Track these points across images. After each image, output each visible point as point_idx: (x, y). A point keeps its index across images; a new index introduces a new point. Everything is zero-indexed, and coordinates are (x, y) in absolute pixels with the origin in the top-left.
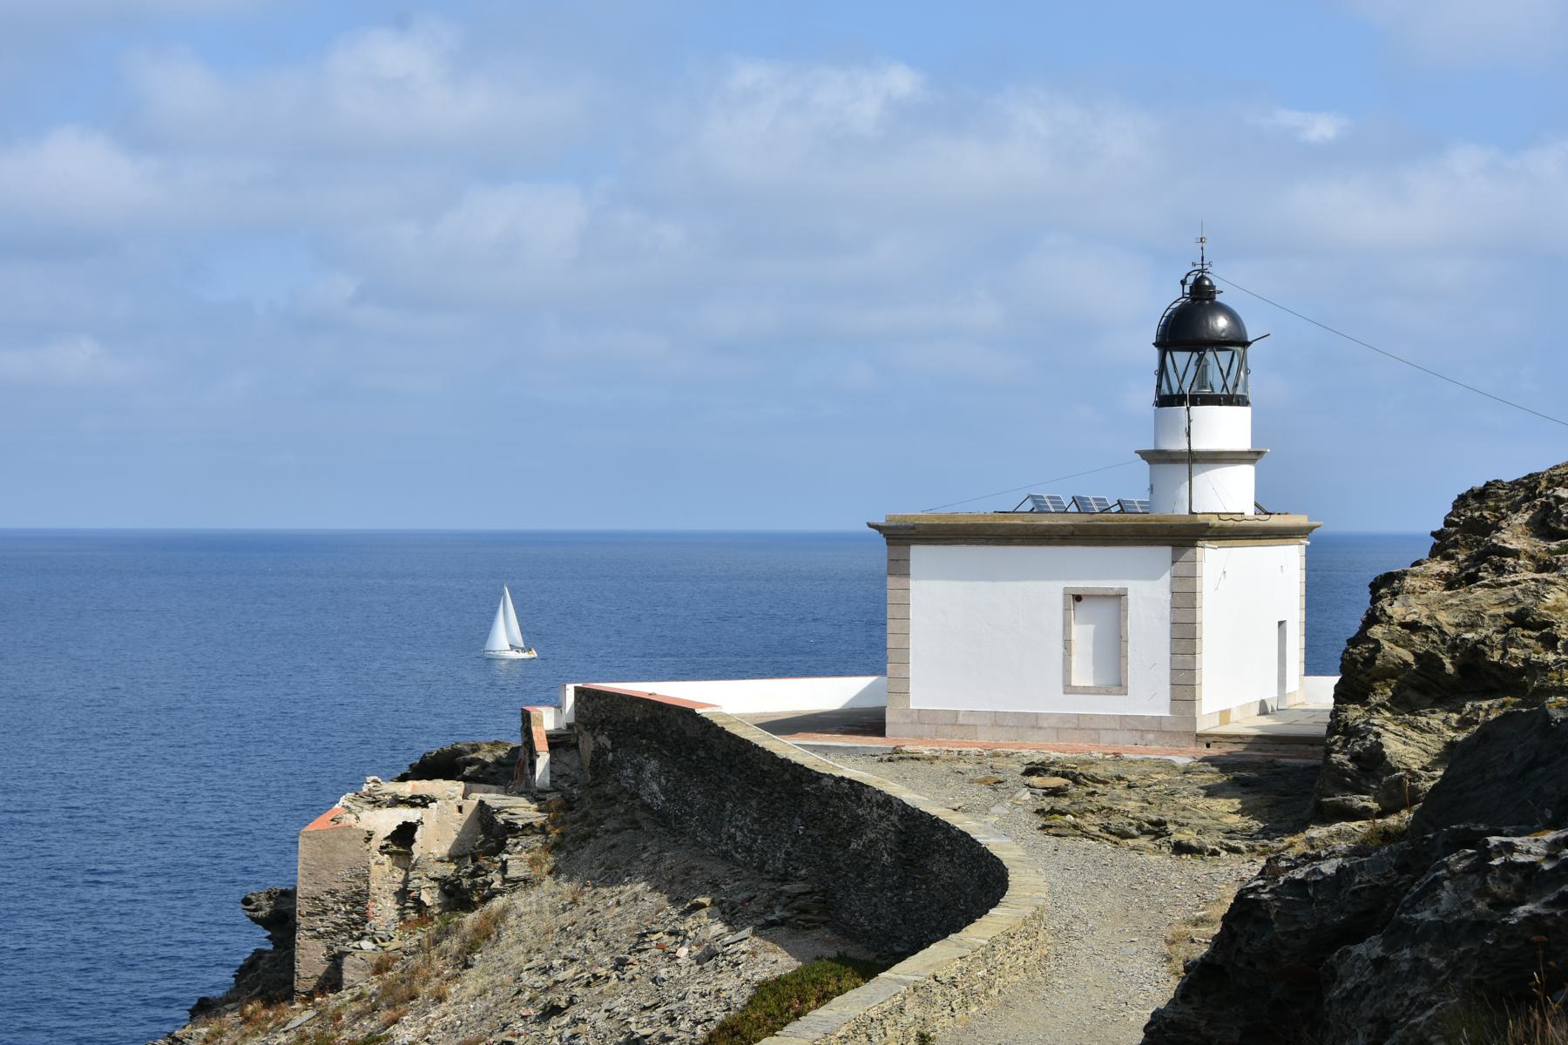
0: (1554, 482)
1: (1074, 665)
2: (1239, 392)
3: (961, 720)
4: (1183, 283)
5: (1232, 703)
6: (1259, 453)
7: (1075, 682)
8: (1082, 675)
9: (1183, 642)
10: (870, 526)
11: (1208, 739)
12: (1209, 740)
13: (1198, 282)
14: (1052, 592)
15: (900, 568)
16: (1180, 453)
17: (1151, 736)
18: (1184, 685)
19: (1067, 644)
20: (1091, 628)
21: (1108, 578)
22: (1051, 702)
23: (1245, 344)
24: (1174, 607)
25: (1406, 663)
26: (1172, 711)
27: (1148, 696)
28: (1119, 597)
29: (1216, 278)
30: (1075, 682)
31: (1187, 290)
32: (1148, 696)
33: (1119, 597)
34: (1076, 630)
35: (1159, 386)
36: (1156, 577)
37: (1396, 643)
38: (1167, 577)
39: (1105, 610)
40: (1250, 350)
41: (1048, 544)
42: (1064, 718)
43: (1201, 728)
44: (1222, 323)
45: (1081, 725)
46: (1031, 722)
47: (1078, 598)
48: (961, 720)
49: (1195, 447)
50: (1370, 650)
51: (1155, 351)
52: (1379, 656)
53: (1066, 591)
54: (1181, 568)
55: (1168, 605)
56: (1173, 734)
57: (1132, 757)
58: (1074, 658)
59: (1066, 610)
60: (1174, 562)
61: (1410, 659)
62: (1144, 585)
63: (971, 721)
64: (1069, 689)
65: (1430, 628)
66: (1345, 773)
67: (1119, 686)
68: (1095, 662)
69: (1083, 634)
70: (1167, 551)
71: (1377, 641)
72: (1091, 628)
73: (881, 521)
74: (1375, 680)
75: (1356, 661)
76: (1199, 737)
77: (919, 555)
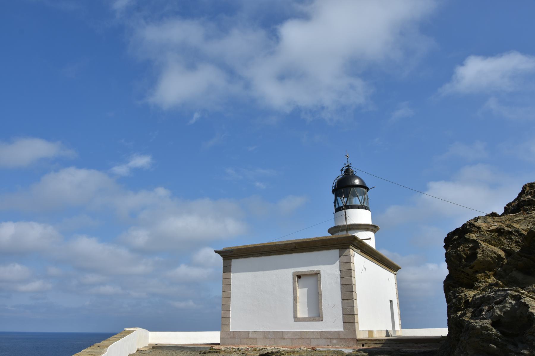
0: (533, 183)
1: (299, 308)
2: (365, 205)
3: (251, 336)
4: (341, 170)
5: (375, 329)
6: (376, 227)
7: (299, 315)
8: (302, 313)
9: (347, 294)
10: (216, 252)
11: (362, 342)
12: (363, 342)
13: (347, 171)
14: (288, 274)
15: (227, 269)
16: (344, 226)
17: (335, 341)
18: (349, 315)
19: (295, 297)
20: (306, 290)
21: (312, 264)
22: (289, 326)
23: (367, 189)
24: (342, 277)
25: (499, 256)
26: (344, 328)
27: (332, 322)
28: (316, 274)
29: (353, 167)
30: (299, 315)
31: (343, 172)
32: (332, 322)
33: (316, 274)
34: (299, 292)
35: (335, 206)
36: (333, 263)
37: (489, 242)
38: (338, 263)
39: (311, 281)
40: (369, 194)
41: (286, 254)
42: (294, 333)
43: (359, 336)
44: (357, 182)
45: (302, 336)
46: (280, 336)
47: (299, 277)
48: (251, 336)
49: (349, 223)
50: (471, 248)
51: (333, 196)
52: (479, 251)
53: (294, 274)
54: (344, 259)
55: (339, 277)
56: (345, 340)
57: (321, 349)
58: (299, 305)
59: (294, 282)
60: (340, 256)
61: (503, 254)
62: (329, 272)
63: (255, 336)
64: (297, 319)
65: (510, 233)
66: (489, 339)
67: (317, 315)
68: (309, 306)
69: (302, 293)
70: (336, 252)
71: (474, 241)
72: (306, 290)
73: (221, 248)
74: (477, 272)
75: (460, 257)
76: (358, 340)
77: (235, 263)
